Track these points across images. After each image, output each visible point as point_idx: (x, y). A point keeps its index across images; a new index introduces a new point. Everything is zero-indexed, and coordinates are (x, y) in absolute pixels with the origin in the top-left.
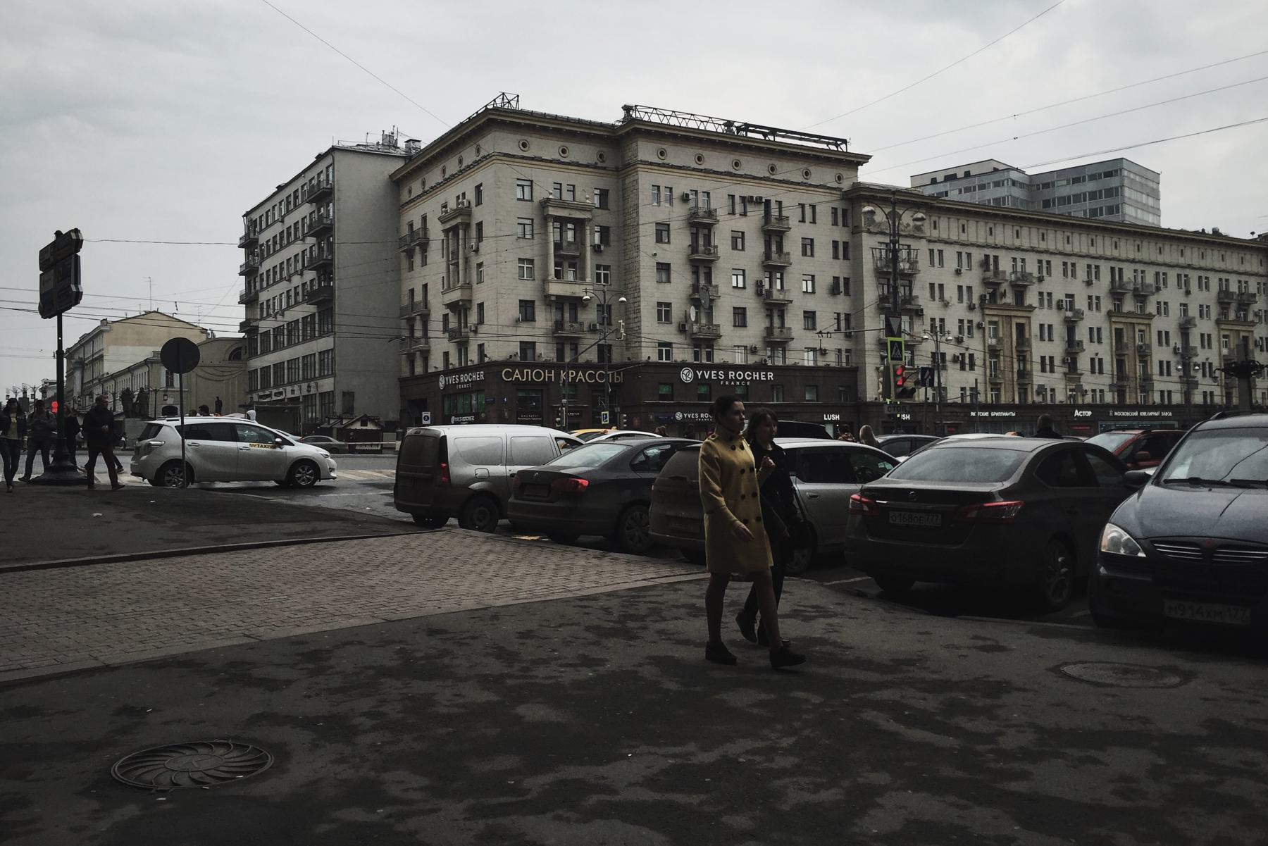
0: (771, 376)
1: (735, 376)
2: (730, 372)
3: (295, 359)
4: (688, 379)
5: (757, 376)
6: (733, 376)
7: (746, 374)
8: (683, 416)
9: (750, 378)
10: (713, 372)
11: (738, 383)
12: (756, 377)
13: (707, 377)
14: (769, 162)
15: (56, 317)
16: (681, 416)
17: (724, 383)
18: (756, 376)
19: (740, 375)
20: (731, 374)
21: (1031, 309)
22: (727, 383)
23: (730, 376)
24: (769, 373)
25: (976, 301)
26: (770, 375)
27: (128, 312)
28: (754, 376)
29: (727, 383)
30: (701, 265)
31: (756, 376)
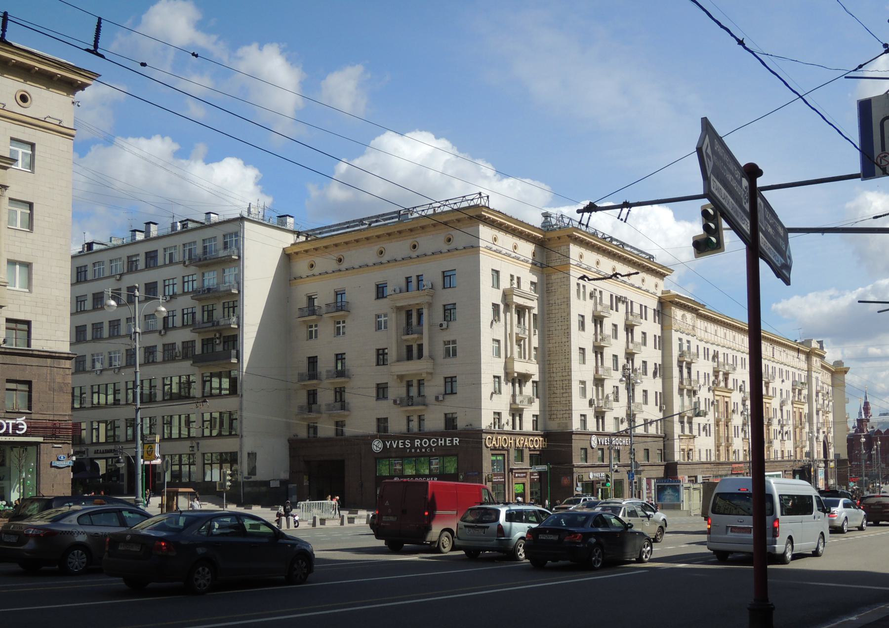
0: (457, 442)
1: (421, 444)
2: (416, 441)
3: (192, 341)
4: (378, 449)
5: (443, 442)
6: (418, 444)
7: (431, 441)
8: (385, 445)
9: (436, 444)
10: (400, 441)
11: (423, 450)
12: (441, 444)
13: (395, 446)
14: (376, 248)
15: (762, 192)
16: (381, 445)
17: (410, 451)
18: (441, 442)
19: (425, 443)
20: (417, 443)
21: (785, 441)
22: (413, 450)
23: (416, 443)
24: (454, 439)
25: (711, 384)
26: (456, 441)
27: (334, 266)
28: (440, 442)
29: (413, 450)
30: (598, 350)
31: (441, 442)
